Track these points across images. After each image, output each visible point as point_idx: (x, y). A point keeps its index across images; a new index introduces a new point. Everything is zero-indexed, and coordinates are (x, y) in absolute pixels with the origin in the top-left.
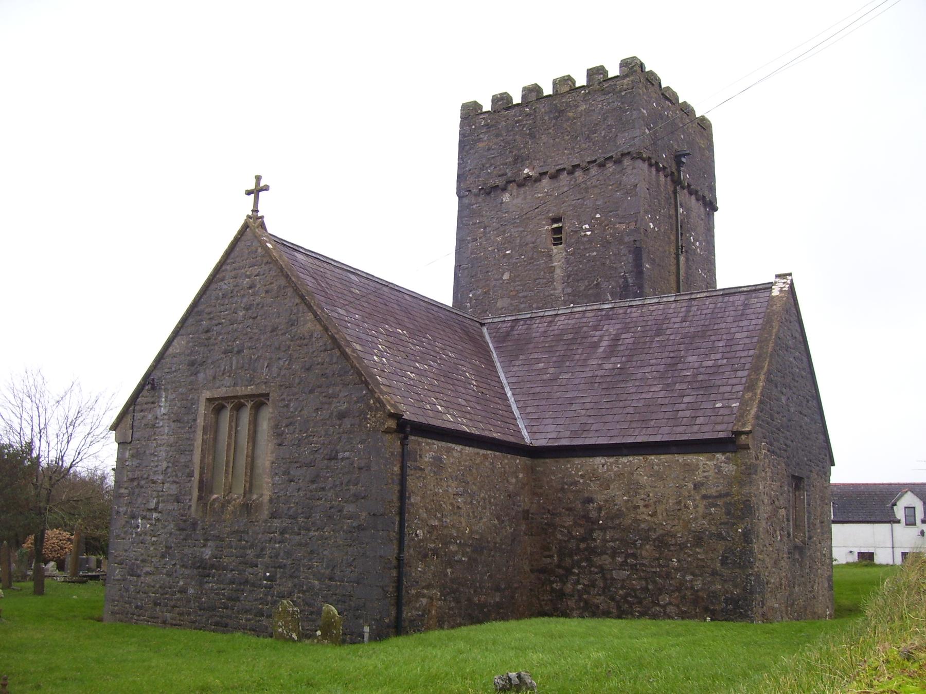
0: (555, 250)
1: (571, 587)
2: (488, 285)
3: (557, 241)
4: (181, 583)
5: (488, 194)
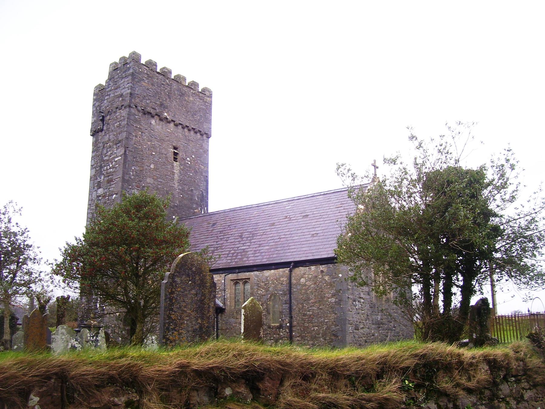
0: (175, 164)
1: (80, 345)
2: (143, 167)
3: (175, 159)
4: (373, 332)
5: (145, 114)
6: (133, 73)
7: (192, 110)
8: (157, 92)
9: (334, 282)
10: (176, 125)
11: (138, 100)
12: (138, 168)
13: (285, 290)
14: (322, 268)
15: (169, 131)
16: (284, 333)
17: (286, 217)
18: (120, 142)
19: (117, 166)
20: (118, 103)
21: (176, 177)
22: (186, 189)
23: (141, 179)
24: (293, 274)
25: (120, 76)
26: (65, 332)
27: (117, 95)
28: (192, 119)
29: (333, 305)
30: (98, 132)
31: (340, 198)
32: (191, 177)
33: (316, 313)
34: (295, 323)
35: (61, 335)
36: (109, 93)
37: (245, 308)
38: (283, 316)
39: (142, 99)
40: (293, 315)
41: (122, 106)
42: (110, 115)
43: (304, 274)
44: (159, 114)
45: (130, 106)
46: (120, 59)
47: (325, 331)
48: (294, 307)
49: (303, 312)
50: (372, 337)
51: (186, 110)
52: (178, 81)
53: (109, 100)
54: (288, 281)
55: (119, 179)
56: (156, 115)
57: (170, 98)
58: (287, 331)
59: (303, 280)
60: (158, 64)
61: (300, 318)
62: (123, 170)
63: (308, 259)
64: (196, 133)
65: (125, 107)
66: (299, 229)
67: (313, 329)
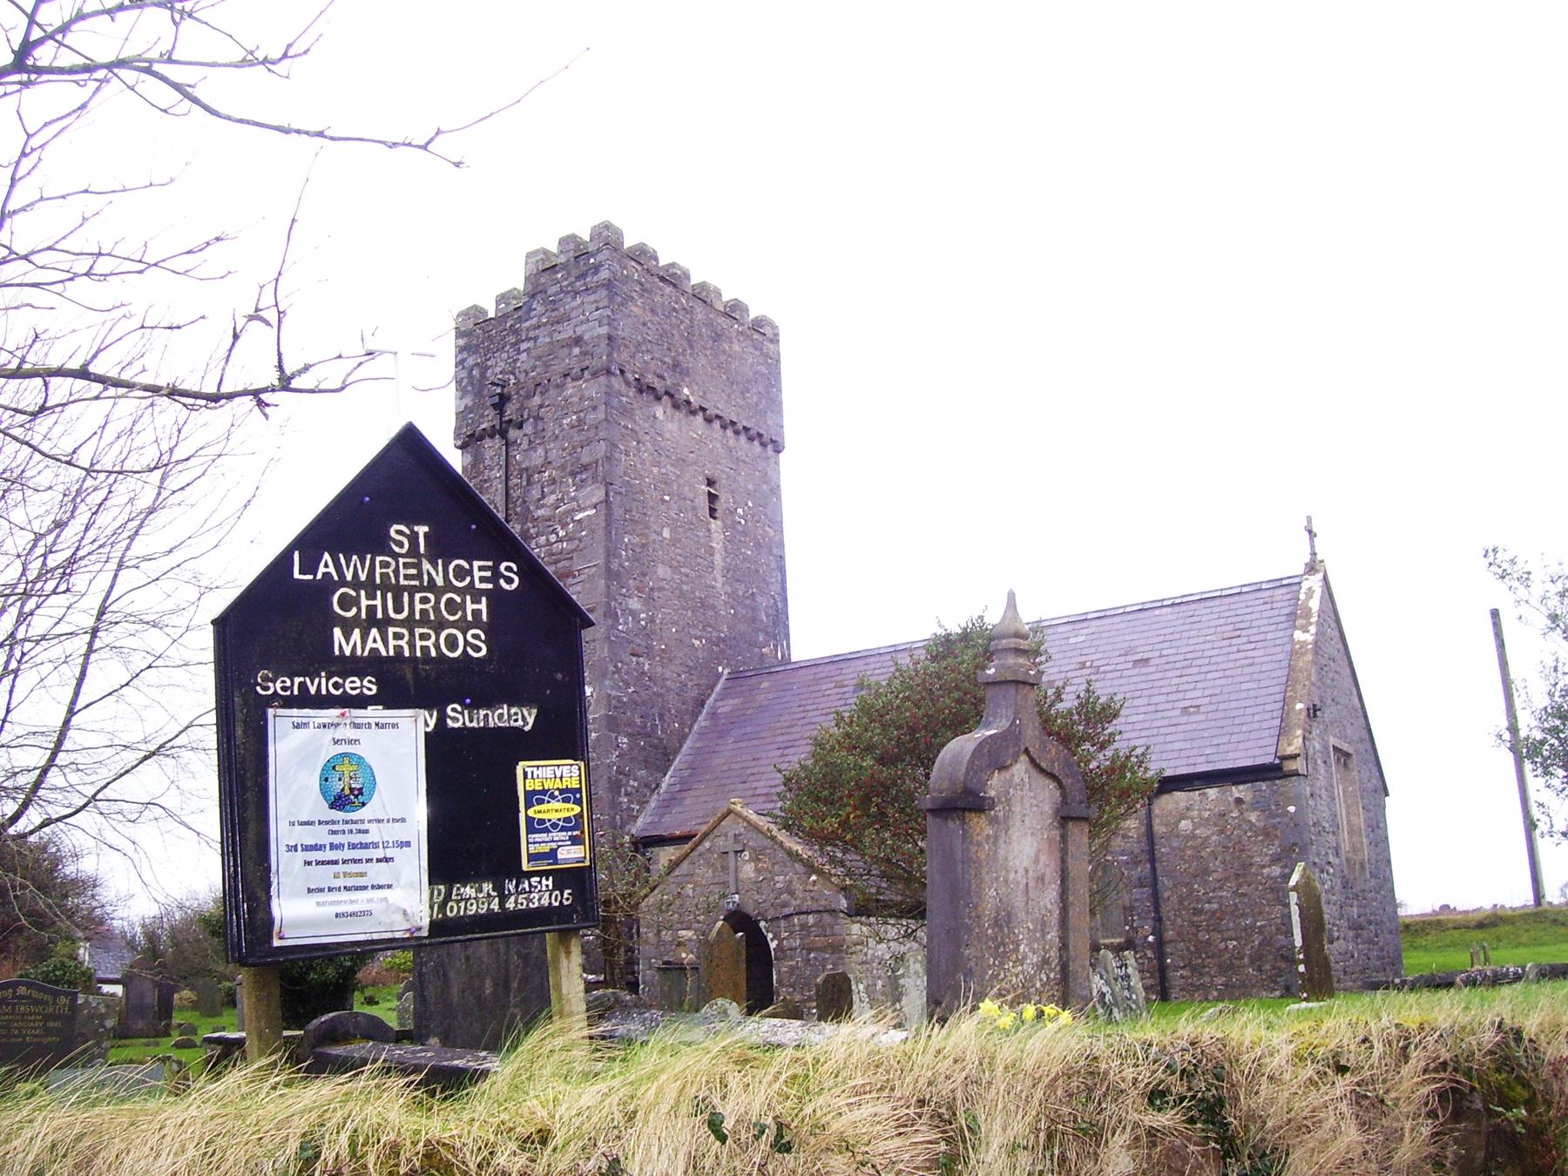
0: (715, 525)
2: (646, 536)
5: (641, 391)
6: (609, 280)
7: (739, 379)
8: (663, 329)
9: (1274, 826)
10: (709, 420)
11: (625, 356)
12: (637, 540)
13: (1137, 851)
14: (1239, 791)
15: (695, 436)
16: (1141, 961)
17: (1083, 666)
18: (585, 468)
19: (584, 533)
20: (571, 359)
21: (718, 559)
22: (741, 593)
23: (645, 569)
24: (1156, 811)
25: (567, 286)
26: (921, 971)
27: (564, 339)
28: (742, 403)
29: (1275, 882)
30: (481, 438)
31: (1227, 614)
32: (746, 559)
33: (1230, 905)
34: (1170, 934)
35: (914, 977)
36: (532, 334)
37: (1294, 889)
38: (1135, 918)
39: (633, 350)
40: (1164, 914)
41: (582, 370)
42: (542, 393)
43: (1188, 809)
44: (672, 392)
45: (609, 372)
46: (563, 241)
47: (1259, 950)
48: (1166, 894)
49: (1192, 906)
50: (1352, 961)
51: (728, 378)
52: (706, 299)
53: (534, 353)
54: (1143, 829)
55: (594, 569)
56: (667, 393)
57: (691, 347)
58: (1150, 954)
59: (1185, 825)
60: (659, 255)
61: (1183, 921)
62: (605, 546)
63: (1240, 765)
64: (751, 439)
65: (595, 375)
66: (1137, 694)
67: (1222, 946)
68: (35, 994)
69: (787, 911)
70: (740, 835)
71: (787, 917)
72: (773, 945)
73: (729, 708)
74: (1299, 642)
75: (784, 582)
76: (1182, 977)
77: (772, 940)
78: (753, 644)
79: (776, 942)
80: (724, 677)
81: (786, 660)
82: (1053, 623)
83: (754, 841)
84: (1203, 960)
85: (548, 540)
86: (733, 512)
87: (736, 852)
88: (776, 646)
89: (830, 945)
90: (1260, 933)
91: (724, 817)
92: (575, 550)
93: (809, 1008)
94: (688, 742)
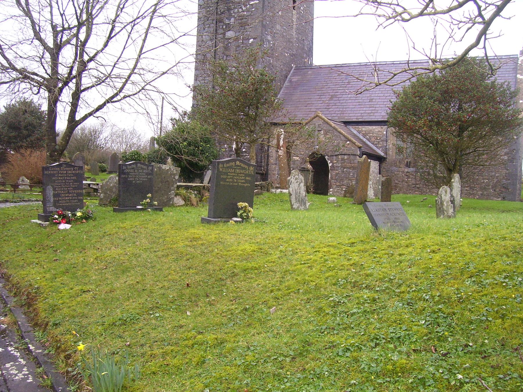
0: (294, 12)
19: (253, 9)
67: (482, 181)
68: (242, 165)
69: (337, 153)
70: (320, 125)
71: (336, 155)
72: (330, 165)
73: (297, 79)
74: (519, 79)
75: (312, 36)
76: (466, 190)
77: (330, 163)
78: (303, 58)
79: (331, 164)
80: (294, 68)
81: (312, 64)
82: (422, 61)
83: (326, 127)
84: (475, 185)
85: (238, 11)
86: (300, 8)
87: (318, 131)
88: (309, 59)
89: (353, 167)
90: (497, 178)
91: (315, 118)
92: (249, 15)
93: (342, 188)
94: (282, 90)
